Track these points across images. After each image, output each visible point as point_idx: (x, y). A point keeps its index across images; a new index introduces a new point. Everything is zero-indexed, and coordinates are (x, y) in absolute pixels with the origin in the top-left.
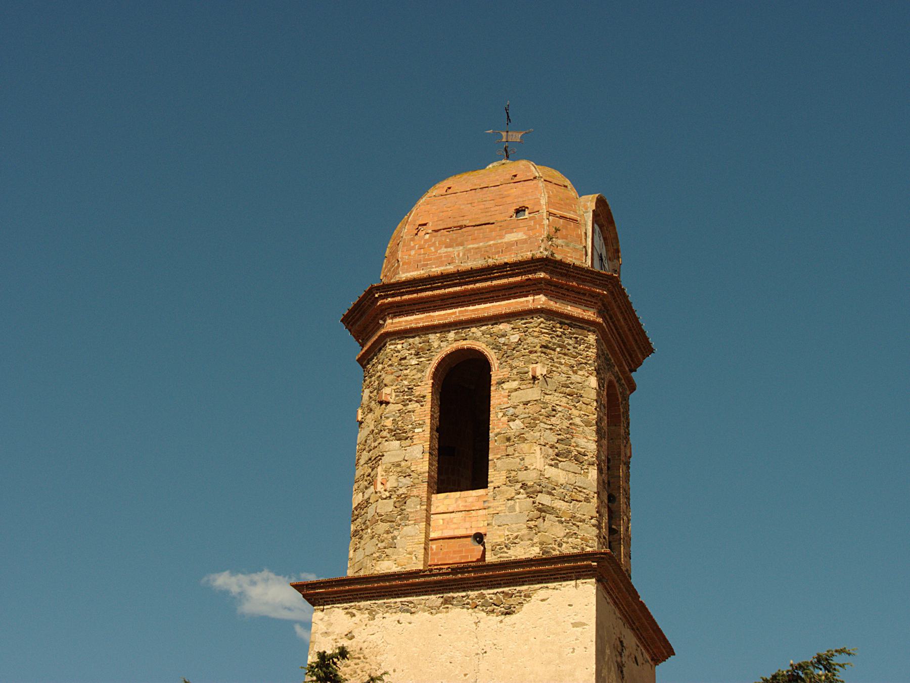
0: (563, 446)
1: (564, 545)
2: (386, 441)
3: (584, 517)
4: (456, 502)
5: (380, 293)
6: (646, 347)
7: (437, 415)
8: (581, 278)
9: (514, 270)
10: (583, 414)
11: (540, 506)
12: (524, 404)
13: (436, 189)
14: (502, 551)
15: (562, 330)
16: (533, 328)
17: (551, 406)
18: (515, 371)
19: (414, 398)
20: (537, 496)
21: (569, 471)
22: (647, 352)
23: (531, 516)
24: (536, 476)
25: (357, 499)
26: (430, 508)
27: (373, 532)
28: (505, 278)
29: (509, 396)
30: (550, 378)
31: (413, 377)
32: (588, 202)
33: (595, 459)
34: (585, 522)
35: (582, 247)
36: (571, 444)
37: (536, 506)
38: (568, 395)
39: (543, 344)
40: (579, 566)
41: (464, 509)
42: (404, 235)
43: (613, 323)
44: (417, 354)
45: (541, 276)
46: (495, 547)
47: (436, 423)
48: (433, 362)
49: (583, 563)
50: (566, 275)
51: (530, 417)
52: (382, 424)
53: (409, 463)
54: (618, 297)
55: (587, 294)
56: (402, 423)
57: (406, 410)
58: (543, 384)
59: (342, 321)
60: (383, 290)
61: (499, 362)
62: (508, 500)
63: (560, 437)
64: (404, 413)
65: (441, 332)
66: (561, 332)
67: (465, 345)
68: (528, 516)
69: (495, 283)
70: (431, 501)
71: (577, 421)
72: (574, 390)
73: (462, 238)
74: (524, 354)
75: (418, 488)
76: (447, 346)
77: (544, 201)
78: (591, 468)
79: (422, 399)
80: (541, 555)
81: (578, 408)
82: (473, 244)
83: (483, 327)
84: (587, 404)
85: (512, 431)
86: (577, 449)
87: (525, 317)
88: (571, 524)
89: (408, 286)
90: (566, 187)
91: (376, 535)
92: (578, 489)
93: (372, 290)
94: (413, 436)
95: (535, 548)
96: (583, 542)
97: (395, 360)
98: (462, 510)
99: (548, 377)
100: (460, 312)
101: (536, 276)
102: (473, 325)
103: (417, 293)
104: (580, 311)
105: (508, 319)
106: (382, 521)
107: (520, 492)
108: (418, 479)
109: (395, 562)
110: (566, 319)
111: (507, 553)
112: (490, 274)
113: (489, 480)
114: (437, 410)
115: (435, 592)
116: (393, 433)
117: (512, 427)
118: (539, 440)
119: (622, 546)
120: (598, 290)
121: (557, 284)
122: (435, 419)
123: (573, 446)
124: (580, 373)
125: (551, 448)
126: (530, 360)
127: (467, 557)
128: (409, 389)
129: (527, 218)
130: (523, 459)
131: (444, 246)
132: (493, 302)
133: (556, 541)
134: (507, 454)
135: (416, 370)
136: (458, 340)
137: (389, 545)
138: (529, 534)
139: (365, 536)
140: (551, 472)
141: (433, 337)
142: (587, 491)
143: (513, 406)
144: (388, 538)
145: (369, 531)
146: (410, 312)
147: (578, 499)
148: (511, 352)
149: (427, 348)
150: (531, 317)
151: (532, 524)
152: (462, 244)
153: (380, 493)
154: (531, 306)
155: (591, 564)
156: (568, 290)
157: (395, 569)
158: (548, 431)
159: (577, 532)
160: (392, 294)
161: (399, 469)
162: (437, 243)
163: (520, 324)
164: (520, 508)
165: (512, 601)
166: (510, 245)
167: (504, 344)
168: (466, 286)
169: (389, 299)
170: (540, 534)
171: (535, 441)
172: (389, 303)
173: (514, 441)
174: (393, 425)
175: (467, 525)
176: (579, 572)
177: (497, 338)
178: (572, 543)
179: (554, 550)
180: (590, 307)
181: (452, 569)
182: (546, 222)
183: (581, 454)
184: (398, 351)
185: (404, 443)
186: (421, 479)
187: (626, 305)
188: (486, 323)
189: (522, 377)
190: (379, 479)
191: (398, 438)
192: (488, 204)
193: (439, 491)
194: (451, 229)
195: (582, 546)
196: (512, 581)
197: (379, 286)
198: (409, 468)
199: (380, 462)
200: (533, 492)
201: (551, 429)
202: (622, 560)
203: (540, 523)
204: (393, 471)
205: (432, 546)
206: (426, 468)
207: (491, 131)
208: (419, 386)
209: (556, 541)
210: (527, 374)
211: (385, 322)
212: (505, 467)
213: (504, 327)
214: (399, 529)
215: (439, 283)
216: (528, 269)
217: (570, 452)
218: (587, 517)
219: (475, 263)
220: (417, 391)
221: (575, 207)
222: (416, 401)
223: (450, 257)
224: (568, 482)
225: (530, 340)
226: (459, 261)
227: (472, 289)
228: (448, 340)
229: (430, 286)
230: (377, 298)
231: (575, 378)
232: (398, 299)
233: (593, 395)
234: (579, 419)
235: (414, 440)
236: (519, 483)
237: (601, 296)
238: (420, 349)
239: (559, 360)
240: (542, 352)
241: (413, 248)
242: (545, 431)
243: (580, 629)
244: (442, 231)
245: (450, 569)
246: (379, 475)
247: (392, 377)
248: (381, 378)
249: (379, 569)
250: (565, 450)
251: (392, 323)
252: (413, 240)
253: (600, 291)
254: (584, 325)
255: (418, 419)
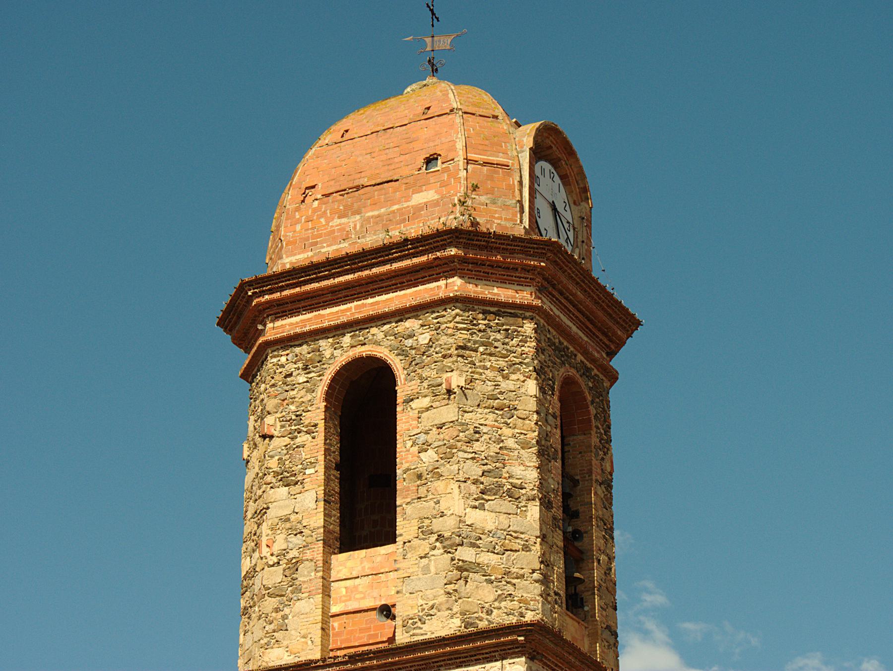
0: (491, 479)
1: (495, 612)
2: (272, 488)
3: (521, 572)
4: (361, 563)
5: (254, 289)
6: (627, 320)
7: (336, 447)
8: (507, 249)
9: (418, 247)
10: (518, 433)
11: (461, 563)
12: (438, 428)
13: (331, 133)
14: (415, 626)
15: (486, 322)
16: (446, 323)
17: (473, 427)
18: (425, 384)
19: (303, 429)
20: (456, 550)
21: (499, 512)
22: (630, 326)
23: (449, 578)
24: (454, 524)
25: (246, 565)
26: (330, 574)
27: (260, 611)
28: (408, 259)
29: (419, 418)
30: (470, 389)
31: (302, 400)
32: (524, 137)
33: (536, 492)
34: (524, 577)
35: (514, 201)
36: (502, 475)
37: (455, 564)
38: (496, 409)
39: (460, 344)
40: (503, 642)
41: (371, 573)
42: (288, 204)
43: (566, 298)
44: (306, 368)
45: (452, 253)
46: (406, 621)
47: (334, 458)
48: (325, 378)
49: (507, 639)
50: (486, 248)
51: (445, 444)
52: (266, 466)
53: (299, 516)
54: (567, 266)
55: (519, 269)
56: (290, 462)
57: (294, 444)
58: (460, 399)
59: (218, 324)
60: (257, 286)
61: (405, 372)
62: (421, 558)
63: (485, 468)
64: (292, 449)
65: (334, 336)
66: (485, 325)
67: (364, 352)
68: (446, 577)
69: (396, 266)
70: (331, 564)
71: (511, 443)
72: (505, 401)
73: (359, 203)
74: (436, 359)
75: (311, 548)
76: (342, 355)
77: (461, 144)
78: (530, 504)
79: (313, 428)
80: (463, 628)
81: (511, 425)
82: (372, 211)
83: (385, 326)
84: (524, 419)
85: (425, 465)
86: (510, 480)
87: (436, 310)
88: (504, 583)
89: (288, 278)
90: (496, 117)
91: (263, 615)
92: (514, 534)
93: (243, 287)
94: (304, 479)
95: (454, 620)
96: (521, 605)
98: (368, 574)
99: (468, 389)
100: (357, 307)
101: (446, 253)
102: (372, 325)
103: (300, 286)
104: (510, 292)
105: (415, 314)
106: (270, 595)
107: (435, 547)
108: (312, 536)
109: (287, 649)
110: (491, 307)
111: (422, 628)
112: (387, 255)
113: (397, 532)
114: (335, 440)
116: (279, 477)
117: (424, 460)
118: (457, 476)
119: (596, 596)
120: (532, 263)
121: (475, 261)
122: (332, 454)
123: (505, 478)
124: (513, 377)
125: (474, 483)
126: (443, 367)
127: (377, 635)
128: (297, 416)
129: (439, 171)
130: (438, 502)
131: (337, 215)
132: (397, 291)
133: (483, 607)
134: (419, 496)
135: (304, 390)
136: (355, 346)
137: (279, 627)
138: (447, 601)
139: (253, 615)
140: (475, 517)
141: (324, 344)
142: (526, 535)
143: (424, 431)
144: (278, 617)
145: (257, 609)
146: (295, 311)
147: (514, 549)
148: (420, 357)
149: (318, 359)
150: (444, 308)
151: (450, 588)
152: (358, 212)
153: (266, 559)
154: (442, 295)
155: (517, 640)
156: (492, 266)
158: (469, 462)
159: (513, 593)
160: (269, 290)
161: (288, 525)
162: (328, 212)
163: (430, 318)
164: (436, 568)
166: (418, 209)
167: (412, 348)
168: (360, 273)
169: (267, 297)
170: (461, 600)
171: (453, 477)
172: (267, 302)
173: (426, 479)
174: (279, 466)
175: (375, 593)
176: (505, 650)
177: (403, 340)
178: (506, 608)
179: (480, 620)
180: (525, 285)
181: (350, 657)
182: (463, 174)
183: (516, 488)
184: (283, 366)
186: (316, 536)
187: (581, 274)
188: (388, 320)
189: (435, 392)
190: (264, 540)
191: (285, 484)
192: (391, 153)
194: (346, 192)
195: (520, 610)
196: (424, 666)
197: (251, 281)
198: (300, 522)
199: (265, 517)
200: (451, 546)
201: (473, 458)
202: (597, 615)
203: (461, 586)
204: (281, 528)
205: (334, 624)
206: (321, 522)
207: (411, 37)
208: (309, 411)
209: (483, 607)
210: (440, 387)
211: (265, 327)
212: (416, 514)
213: (411, 324)
214: (290, 605)
215: (326, 271)
216: (435, 245)
217: (501, 486)
219: (375, 237)
220: (307, 419)
221: (506, 146)
222: (306, 432)
223: (344, 231)
224: (499, 528)
225: (444, 339)
226: (356, 234)
227: (368, 277)
228: (342, 347)
229: (315, 276)
230: (250, 295)
231: (505, 385)
232: (277, 295)
233: (532, 405)
234: (513, 440)
235: (305, 485)
236: (434, 534)
237: (539, 270)
238: (308, 360)
239: (483, 364)
240: (458, 356)
241: (298, 221)
242: (465, 462)
244: (334, 194)
245: (347, 657)
246: (264, 535)
247: (276, 401)
248: (264, 402)
249: (268, 660)
250: (493, 484)
251: (274, 327)
252: (298, 209)
253: (536, 263)
254: (518, 311)
255: (309, 456)
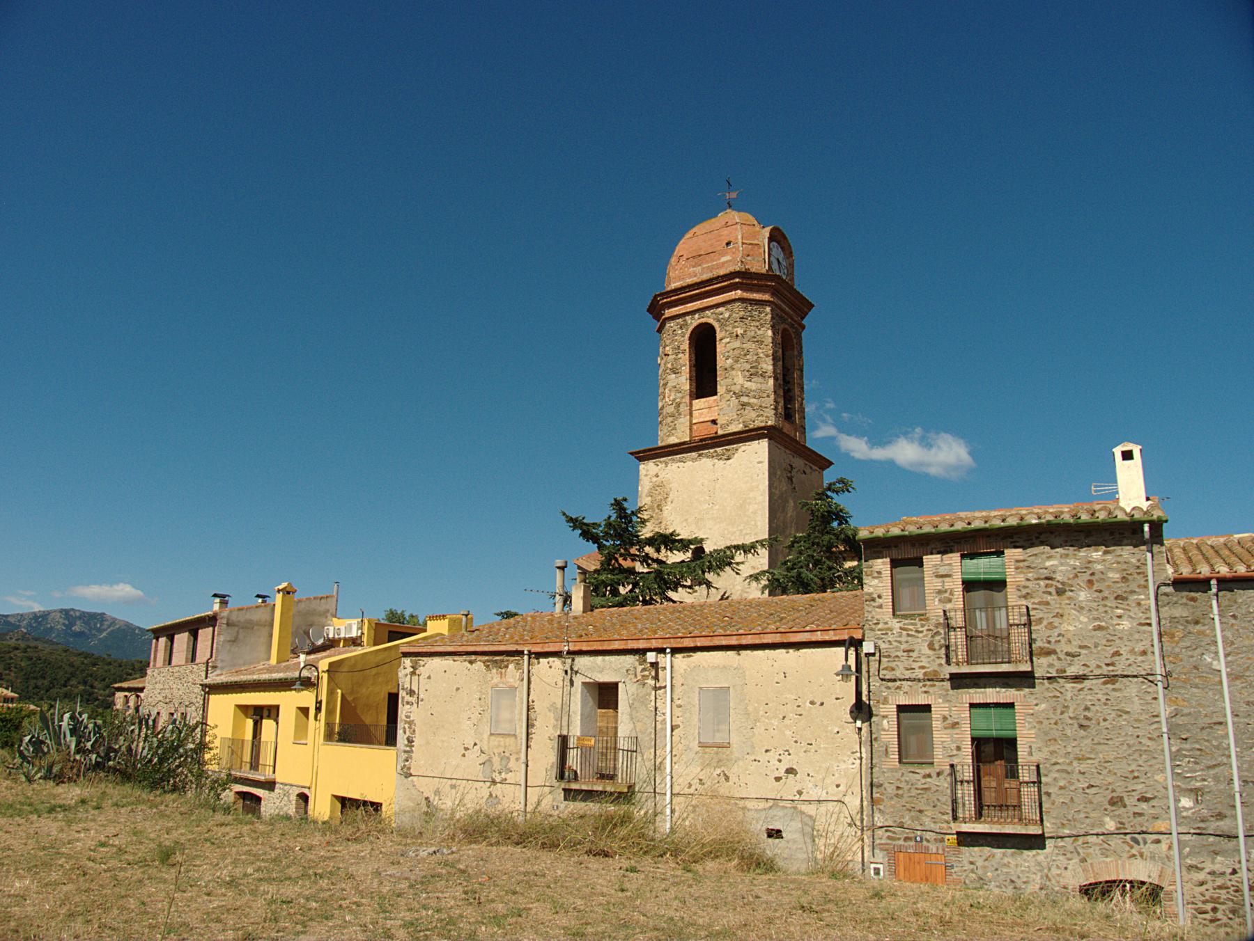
7: (693, 359)
25: (660, 405)
44: (681, 328)
69: (715, 286)
71: (761, 355)
93: (656, 296)
97: (671, 332)
104: (761, 296)
114: (693, 355)
115: (694, 451)
140: (748, 384)
151: (739, 412)
152: (700, 265)
154: (733, 297)
157: (677, 441)
165: (730, 453)
166: (723, 264)
185: (677, 375)
192: (713, 241)
193: (697, 398)
206: (688, 388)
218: (768, 405)
225: (734, 315)
232: (669, 299)
233: (770, 340)
243: (760, 465)
